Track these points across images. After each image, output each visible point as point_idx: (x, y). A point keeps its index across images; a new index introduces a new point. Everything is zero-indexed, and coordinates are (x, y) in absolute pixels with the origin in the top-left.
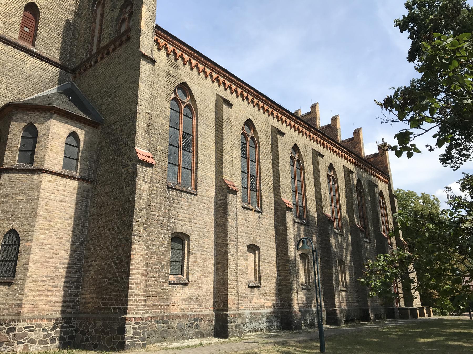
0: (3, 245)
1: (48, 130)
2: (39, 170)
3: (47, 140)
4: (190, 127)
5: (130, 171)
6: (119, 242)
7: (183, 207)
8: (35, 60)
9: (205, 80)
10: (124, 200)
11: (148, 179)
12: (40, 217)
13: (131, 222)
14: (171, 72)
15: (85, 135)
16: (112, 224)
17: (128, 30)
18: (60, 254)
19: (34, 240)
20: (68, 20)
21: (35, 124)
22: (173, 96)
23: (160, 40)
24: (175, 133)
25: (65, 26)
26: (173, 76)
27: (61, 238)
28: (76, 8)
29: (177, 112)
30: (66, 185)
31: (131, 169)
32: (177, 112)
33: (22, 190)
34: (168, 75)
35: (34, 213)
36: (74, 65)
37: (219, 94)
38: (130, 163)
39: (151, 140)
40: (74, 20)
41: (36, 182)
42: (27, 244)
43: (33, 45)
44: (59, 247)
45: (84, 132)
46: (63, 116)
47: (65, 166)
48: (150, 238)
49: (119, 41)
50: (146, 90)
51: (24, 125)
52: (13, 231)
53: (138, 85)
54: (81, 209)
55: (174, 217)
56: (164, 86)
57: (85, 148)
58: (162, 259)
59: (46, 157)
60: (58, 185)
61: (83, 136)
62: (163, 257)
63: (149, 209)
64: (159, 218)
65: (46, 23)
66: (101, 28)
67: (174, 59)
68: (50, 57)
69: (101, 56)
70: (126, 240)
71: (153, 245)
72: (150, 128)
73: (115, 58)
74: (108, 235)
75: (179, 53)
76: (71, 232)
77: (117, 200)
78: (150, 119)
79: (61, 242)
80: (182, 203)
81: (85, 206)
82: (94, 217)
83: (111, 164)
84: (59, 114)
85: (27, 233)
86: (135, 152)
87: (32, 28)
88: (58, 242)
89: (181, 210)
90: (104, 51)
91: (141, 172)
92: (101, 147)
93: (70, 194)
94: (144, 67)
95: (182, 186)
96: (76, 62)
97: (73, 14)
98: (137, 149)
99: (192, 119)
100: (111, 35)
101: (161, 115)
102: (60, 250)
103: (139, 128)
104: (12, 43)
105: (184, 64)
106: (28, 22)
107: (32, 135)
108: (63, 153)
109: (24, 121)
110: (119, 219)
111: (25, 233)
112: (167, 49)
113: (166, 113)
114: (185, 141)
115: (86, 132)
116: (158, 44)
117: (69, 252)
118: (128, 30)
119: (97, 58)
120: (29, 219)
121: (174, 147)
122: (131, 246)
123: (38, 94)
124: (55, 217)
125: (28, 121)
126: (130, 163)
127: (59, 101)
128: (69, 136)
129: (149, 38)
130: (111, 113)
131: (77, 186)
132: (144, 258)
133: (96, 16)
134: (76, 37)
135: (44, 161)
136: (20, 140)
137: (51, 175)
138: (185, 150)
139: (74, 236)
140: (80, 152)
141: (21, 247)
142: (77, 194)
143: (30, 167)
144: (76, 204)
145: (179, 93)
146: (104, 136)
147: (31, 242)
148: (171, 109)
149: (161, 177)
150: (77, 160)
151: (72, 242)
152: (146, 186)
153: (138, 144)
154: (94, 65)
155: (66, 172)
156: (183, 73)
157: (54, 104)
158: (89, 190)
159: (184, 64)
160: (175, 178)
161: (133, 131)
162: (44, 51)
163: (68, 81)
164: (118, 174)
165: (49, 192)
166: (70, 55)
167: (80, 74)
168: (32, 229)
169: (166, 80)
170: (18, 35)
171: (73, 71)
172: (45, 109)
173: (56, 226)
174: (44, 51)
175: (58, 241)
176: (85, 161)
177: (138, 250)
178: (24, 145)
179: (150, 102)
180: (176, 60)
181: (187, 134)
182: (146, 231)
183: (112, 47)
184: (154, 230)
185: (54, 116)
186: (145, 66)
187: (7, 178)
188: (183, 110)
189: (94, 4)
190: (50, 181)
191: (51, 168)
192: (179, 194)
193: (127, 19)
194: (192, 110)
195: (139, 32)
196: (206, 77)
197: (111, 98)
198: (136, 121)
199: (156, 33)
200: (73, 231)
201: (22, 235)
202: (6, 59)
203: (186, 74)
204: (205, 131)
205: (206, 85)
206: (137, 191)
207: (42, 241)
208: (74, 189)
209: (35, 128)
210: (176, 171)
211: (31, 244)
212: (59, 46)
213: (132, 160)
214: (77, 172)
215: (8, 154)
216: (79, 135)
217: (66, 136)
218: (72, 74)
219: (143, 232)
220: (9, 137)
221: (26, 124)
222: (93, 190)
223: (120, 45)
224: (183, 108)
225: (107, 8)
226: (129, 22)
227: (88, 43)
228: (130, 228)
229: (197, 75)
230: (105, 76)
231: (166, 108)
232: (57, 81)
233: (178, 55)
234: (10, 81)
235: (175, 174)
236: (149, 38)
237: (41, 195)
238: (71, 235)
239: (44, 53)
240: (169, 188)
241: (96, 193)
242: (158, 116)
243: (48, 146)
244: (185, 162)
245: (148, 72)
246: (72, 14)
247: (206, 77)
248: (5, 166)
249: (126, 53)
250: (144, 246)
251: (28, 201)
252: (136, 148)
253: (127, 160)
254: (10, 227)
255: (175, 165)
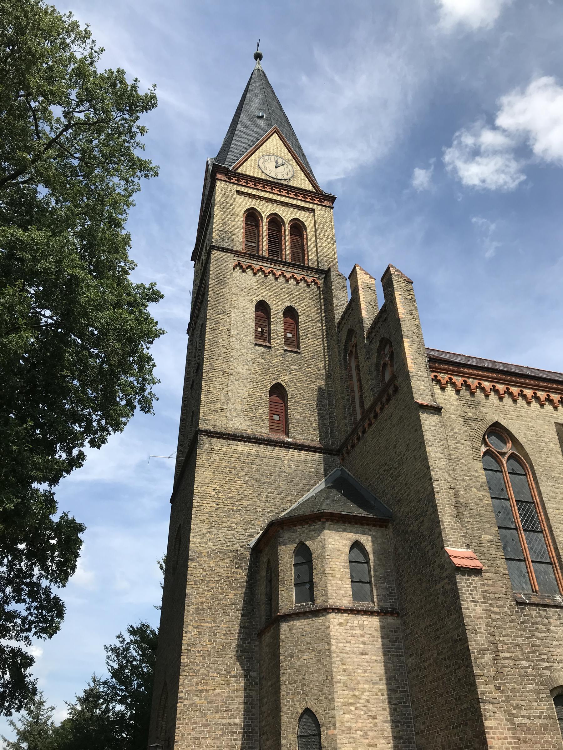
0: (300, 736)
1: (323, 547)
2: (322, 609)
3: (325, 562)
4: (526, 491)
5: (448, 587)
6: (462, 716)
7: (556, 636)
8: (293, 452)
9: (529, 408)
10: (452, 638)
11: (478, 596)
12: (339, 685)
13: (472, 678)
14: (470, 414)
15: (372, 542)
16: (443, 682)
17: (394, 378)
18: (378, 746)
19: (338, 724)
20: (320, 388)
21: (306, 543)
22: (483, 449)
23: (440, 376)
24: (503, 507)
25: (318, 397)
26: (475, 420)
27: (374, 718)
28: (326, 370)
29: (496, 471)
30: (363, 626)
31: (449, 584)
32: (496, 471)
33: (307, 643)
34: (466, 420)
35: (329, 679)
36: (338, 444)
37: (559, 421)
38: (444, 575)
39: (467, 529)
40: (327, 384)
41: (323, 628)
42: (330, 732)
43: (287, 434)
44: (375, 734)
45: (370, 538)
46: (338, 521)
47: (356, 596)
48: (514, 703)
49: (385, 395)
50: (439, 455)
51: (293, 547)
52: (308, 712)
53: (425, 450)
54: (393, 662)
55: (545, 657)
56: (465, 438)
57: (377, 562)
58: (547, 742)
59: (329, 588)
60: (352, 628)
61: (371, 544)
62: (547, 737)
63: (496, 649)
64: (517, 662)
65: (296, 402)
66: (361, 384)
67: (469, 394)
68: (308, 443)
69: (367, 422)
70: (472, 713)
71: (523, 717)
72: (460, 510)
73: (386, 420)
74: (443, 706)
75: (473, 383)
76: (387, 705)
77: (440, 641)
78: (457, 496)
79: (376, 725)
80: (552, 628)
81: (397, 656)
82: (414, 674)
83: (418, 581)
84: (332, 521)
85: (327, 714)
86: (446, 555)
87: (282, 414)
88: (371, 725)
89: (554, 642)
90: (371, 414)
91: (464, 587)
92: (399, 555)
93: (371, 639)
94: (427, 422)
95: (542, 597)
96: (341, 438)
97: (324, 378)
98: (449, 549)
99: (526, 475)
100: (374, 391)
101: (472, 484)
102: (377, 738)
103: (443, 515)
104: (264, 440)
105: (487, 396)
106: (277, 407)
107: (305, 558)
108: (349, 577)
109: (293, 541)
110: (452, 675)
111: (324, 713)
112: (454, 384)
113: (479, 480)
114: (525, 515)
115: (373, 537)
116: (438, 382)
117: (392, 741)
118: (394, 378)
119: (364, 426)
120: (326, 690)
121: (507, 530)
122: (482, 725)
123: (304, 496)
124: (358, 682)
125: (297, 540)
126: (444, 575)
127: (329, 502)
128: (351, 549)
129: (424, 379)
130: (399, 500)
131: (379, 624)
132: (510, 743)
133: (351, 370)
134: (333, 405)
135: (326, 595)
136: (293, 570)
137: (340, 614)
138: (530, 531)
139: (393, 711)
140: (372, 570)
141: (323, 737)
142: (382, 637)
143: (312, 607)
144: (385, 655)
145: (493, 441)
146: (399, 538)
147: (335, 728)
148: (485, 469)
149: (500, 587)
150: (370, 583)
151: (393, 721)
152: (479, 610)
153: (449, 541)
154: (363, 436)
155: (359, 605)
156: (489, 410)
157: (323, 508)
158: (398, 628)
159: (487, 396)
160: (526, 583)
161: (436, 523)
162: (299, 437)
163: (337, 466)
164: (431, 595)
165: (342, 641)
166: (332, 432)
167: (348, 453)
168: (332, 706)
169: (465, 429)
170: (268, 428)
171: (338, 452)
172: (312, 519)
173: (363, 697)
174: (299, 437)
175: (371, 723)
176: (382, 583)
177: (497, 728)
178: (299, 576)
179: (449, 470)
180: (472, 394)
181: (524, 502)
182: (502, 692)
183: (379, 405)
184: (516, 686)
185: (327, 524)
186: (428, 421)
187: (288, 629)
188: (505, 465)
189: (345, 356)
190: (340, 624)
191: (338, 604)
192: (542, 613)
193: (389, 362)
194: (521, 461)
195: (407, 376)
196: (529, 403)
197: (394, 478)
198: (436, 506)
199: (432, 369)
200: (389, 702)
201: (321, 720)
202: (260, 463)
203: (494, 409)
204: (553, 489)
205: (533, 415)
206: (467, 620)
207: (348, 724)
208: (376, 630)
209: (307, 548)
210: (524, 570)
211: (336, 732)
212: (316, 425)
213: (446, 570)
214: (374, 602)
215: (283, 592)
216: (364, 544)
217: (347, 550)
218: (338, 455)
219: (497, 694)
220: (280, 569)
221: (296, 545)
222: (403, 627)
223: (388, 400)
224: (504, 462)
225: (362, 358)
226: (392, 366)
227: (349, 408)
228: (473, 688)
229: (513, 405)
230: (380, 449)
231: (477, 471)
232: (322, 471)
233: (473, 386)
234: (270, 490)
235: (524, 576)
236: (424, 379)
237: (333, 647)
238: (388, 709)
239: (301, 439)
240: (520, 604)
241: (408, 631)
242: (469, 487)
243: (328, 570)
244: (535, 552)
245: (434, 428)
246: (322, 379)
247: (529, 403)
248: (282, 612)
249: (399, 409)
250: (505, 722)
251: (319, 660)
252: (447, 548)
253: (439, 570)
254: (304, 705)
255: (520, 560)
